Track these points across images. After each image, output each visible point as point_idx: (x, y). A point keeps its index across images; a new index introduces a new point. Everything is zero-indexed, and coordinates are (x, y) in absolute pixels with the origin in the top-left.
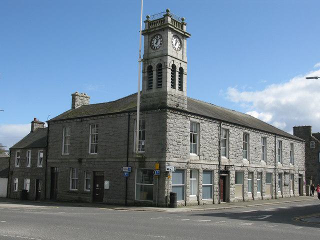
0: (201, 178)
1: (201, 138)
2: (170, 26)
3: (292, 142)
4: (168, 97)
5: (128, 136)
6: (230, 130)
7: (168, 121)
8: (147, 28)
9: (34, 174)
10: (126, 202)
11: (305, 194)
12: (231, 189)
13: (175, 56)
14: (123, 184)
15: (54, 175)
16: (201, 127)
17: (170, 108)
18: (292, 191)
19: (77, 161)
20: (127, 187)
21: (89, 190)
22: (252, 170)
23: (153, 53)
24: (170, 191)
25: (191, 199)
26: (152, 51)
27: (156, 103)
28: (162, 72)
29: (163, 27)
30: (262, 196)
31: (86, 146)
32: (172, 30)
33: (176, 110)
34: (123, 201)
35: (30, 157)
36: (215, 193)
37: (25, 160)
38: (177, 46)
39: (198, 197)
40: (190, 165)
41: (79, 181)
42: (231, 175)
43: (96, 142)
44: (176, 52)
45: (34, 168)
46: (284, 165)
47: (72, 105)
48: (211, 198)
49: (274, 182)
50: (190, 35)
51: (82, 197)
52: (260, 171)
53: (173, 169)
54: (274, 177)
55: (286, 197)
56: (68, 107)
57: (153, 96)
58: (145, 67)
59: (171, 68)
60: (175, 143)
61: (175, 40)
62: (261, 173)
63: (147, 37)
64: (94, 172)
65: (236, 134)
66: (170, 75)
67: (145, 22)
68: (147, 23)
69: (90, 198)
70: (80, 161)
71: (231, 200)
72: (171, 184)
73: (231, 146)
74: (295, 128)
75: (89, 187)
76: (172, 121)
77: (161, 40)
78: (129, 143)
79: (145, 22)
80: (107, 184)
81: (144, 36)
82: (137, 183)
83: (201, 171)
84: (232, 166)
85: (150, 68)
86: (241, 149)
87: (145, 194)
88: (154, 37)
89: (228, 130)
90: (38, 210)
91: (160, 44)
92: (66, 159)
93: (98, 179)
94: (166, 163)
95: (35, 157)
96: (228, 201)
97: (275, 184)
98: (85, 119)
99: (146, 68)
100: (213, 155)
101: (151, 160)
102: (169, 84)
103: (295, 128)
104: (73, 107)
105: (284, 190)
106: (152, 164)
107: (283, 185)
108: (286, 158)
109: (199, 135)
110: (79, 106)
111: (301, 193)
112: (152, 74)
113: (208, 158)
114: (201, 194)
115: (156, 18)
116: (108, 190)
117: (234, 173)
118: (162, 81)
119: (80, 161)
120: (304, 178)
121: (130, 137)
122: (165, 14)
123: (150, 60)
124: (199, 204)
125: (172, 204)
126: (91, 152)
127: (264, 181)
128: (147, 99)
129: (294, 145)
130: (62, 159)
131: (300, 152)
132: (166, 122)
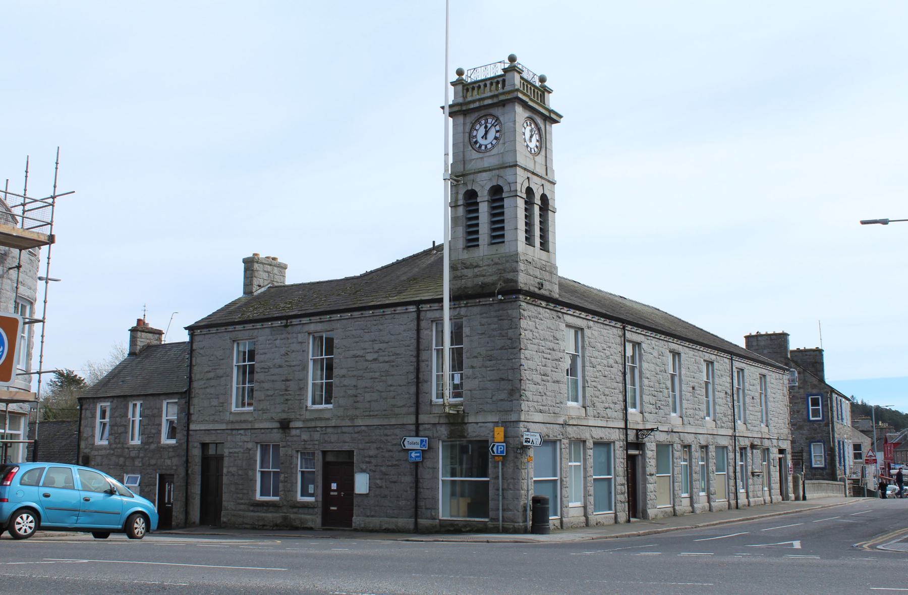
0: (590, 461)
1: (587, 364)
2: (520, 95)
3: (764, 372)
4: (522, 266)
5: (418, 362)
6: (643, 345)
7: (523, 323)
8: (460, 100)
9: (153, 462)
10: (416, 523)
11: (792, 496)
12: (650, 487)
13: (530, 166)
14: (408, 479)
15: (211, 464)
16: (586, 338)
17: (528, 293)
18: (766, 489)
19: (277, 425)
20: (417, 488)
21: (312, 499)
22: (689, 439)
23: (476, 161)
24: (532, 494)
25: (571, 514)
26: (475, 155)
27: (488, 280)
28: (502, 207)
29: (502, 98)
30: (709, 502)
31: (301, 389)
33: (535, 297)
34: (409, 523)
35: (138, 418)
36: (618, 496)
37: (126, 426)
38: (533, 144)
39: (585, 507)
40: (569, 429)
41: (282, 477)
42: (649, 454)
43: (251, 381)
44: (531, 157)
45: (153, 446)
46: (749, 426)
47: (245, 285)
48: (610, 509)
49: (731, 469)
50: (561, 117)
51: (292, 516)
52: (703, 443)
53: (537, 439)
54: (731, 455)
55: (757, 505)
56: (236, 292)
57: (481, 263)
58: (457, 193)
59: (524, 196)
60: (537, 378)
61: (528, 128)
62: (705, 448)
63: (461, 119)
64: (324, 453)
65: (655, 354)
66: (524, 213)
67: (453, 84)
68: (460, 87)
69: (316, 519)
70: (285, 425)
71: (651, 512)
72: (532, 478)
73: (646, 382)
74: (747, 338)
75: (311, 491)
76: (530, 323)
77: (498, 128)
78: (419, 379)
79: (453, 84)
80: (361, 483)
81: (451, 120)
83: (590, 444)
84: (652, 430)
85: (471, 196)
86: (666, 391)
87: (463, 503)
88: (478, 121)
89: (639, 344)
91: (496, 138)
92: (245, 422)
93: (338, 468)
95: (151, 420)
96: (645, 516)
97: (735, 472)
98: (295, 321)
99: (461, 196)
100: (612, 406)
101: (480, 419)
102: (522, 235)
103: (747, 338)
105: (751, 488)
106: (483, 425)
107: (749, 474)
108: (753, 412)
109: (583, 357)
110: (263, 290)
111: (785, 497)
112: (477, 211)
113: (603, 413)
114: (591, 499)
115: (480, 76)
116: (366, 495)
117: (654, 448)
118: (503, 228)
119: (285, 425)
120: (789, 457)
121: (423, 365)
122: (507, 66)
123: (471, 177)
124: (587, 524)
125: (539, 525)
126: (314, 403)
127: (712, 467)
128: (465, 272)
129: (768, 378)
130: (232, 422)
131: (779, 396)
132: (517, 327)
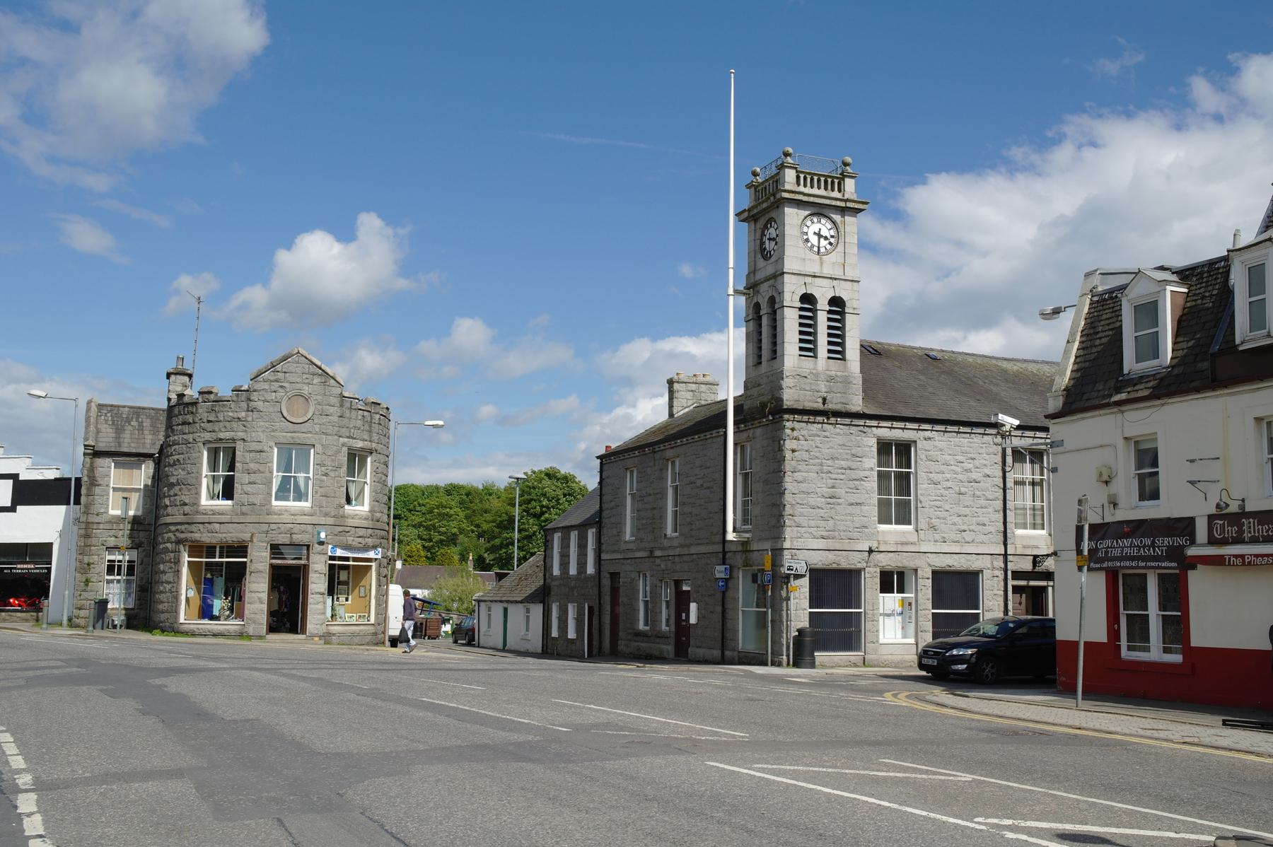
32: (799, 204)
56: (663, 417)
82: (1147, 649)
85: (757, 307)
90: (283, 642)
91: (807, 240)
94: (786, 552)
104: (671, 415)
